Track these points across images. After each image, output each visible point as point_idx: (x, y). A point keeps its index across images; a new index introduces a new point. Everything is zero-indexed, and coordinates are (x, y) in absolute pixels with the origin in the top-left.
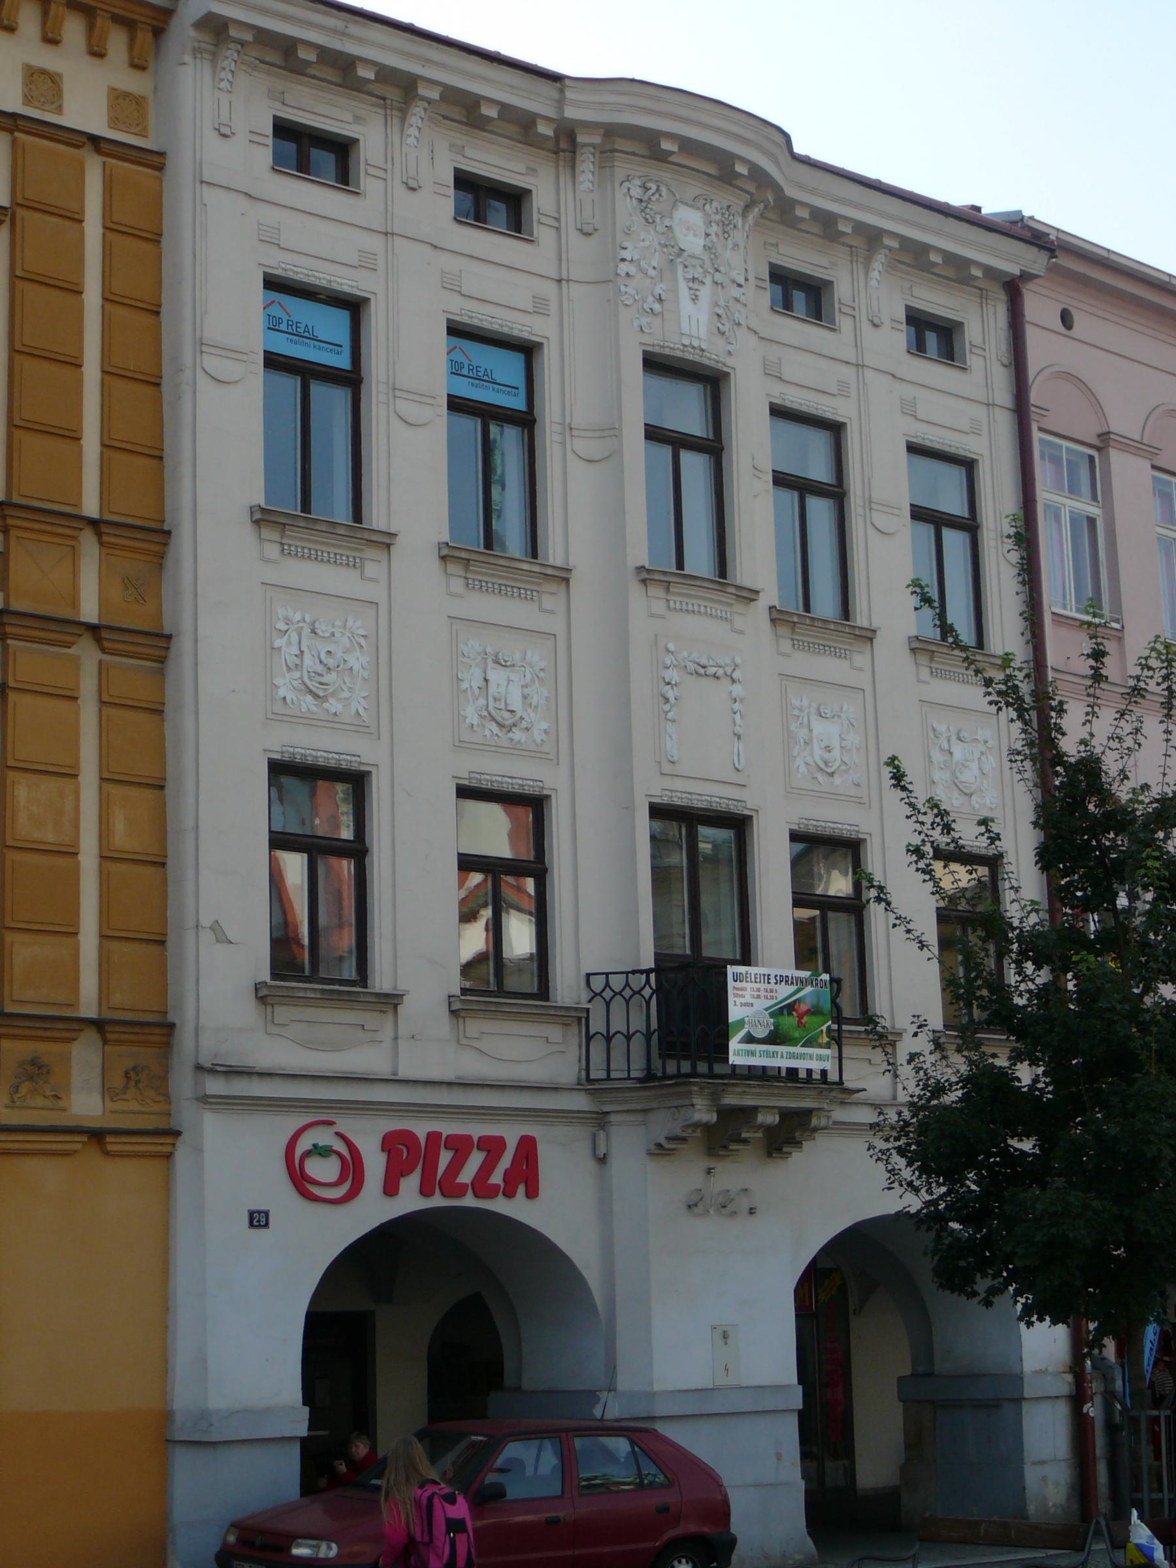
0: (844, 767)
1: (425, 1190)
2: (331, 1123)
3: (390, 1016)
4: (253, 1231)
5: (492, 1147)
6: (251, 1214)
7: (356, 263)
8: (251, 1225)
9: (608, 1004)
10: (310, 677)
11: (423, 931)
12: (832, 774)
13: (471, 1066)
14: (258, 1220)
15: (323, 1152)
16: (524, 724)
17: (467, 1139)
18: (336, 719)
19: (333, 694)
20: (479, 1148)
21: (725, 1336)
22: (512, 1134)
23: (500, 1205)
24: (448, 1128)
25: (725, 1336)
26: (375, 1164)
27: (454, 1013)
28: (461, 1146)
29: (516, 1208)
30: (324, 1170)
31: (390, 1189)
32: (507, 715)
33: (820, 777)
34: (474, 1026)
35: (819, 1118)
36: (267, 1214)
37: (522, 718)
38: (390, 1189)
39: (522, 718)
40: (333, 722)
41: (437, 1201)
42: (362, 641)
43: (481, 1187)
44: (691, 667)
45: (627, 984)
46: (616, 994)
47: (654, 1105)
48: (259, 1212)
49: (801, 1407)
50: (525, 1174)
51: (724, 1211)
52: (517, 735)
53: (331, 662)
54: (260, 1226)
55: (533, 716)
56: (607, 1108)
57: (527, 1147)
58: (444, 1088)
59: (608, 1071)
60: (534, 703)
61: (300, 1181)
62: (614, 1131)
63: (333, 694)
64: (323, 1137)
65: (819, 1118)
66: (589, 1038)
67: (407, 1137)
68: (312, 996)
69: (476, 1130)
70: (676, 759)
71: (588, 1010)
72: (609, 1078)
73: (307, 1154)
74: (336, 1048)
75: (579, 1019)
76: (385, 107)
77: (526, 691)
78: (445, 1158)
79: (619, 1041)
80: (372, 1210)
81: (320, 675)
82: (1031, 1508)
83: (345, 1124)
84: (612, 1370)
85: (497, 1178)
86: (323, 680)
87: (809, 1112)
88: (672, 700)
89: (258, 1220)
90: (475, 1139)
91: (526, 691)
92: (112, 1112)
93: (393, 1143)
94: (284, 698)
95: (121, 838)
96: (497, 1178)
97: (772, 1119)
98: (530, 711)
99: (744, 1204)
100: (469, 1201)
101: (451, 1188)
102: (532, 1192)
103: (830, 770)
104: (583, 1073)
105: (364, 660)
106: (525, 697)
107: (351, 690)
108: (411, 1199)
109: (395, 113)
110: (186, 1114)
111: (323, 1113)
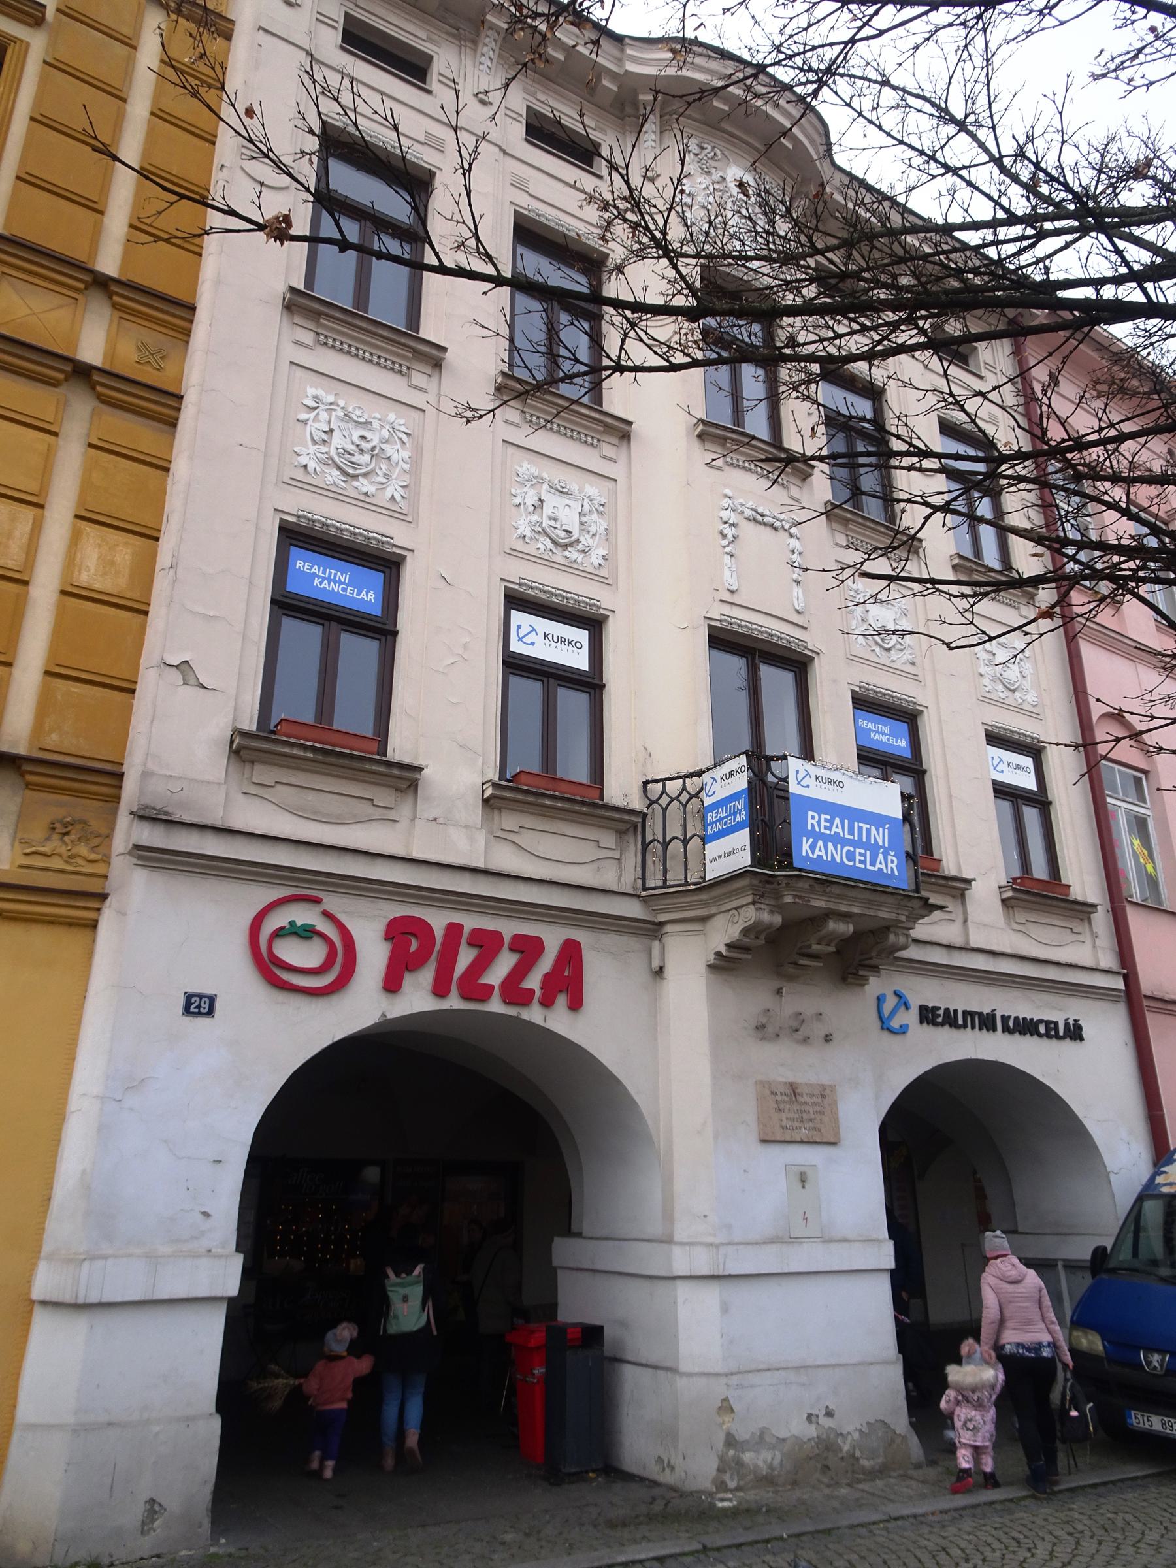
0: (898, 646)
1: (440, 989)
2: (317, 901)
3: (410, 799)
4: (188, 1019)
5: (529, 949)
6: (189, 998)
7: (422, 140)
8: (187, 1011)
9: (665, 810)
10: (338, 454)
11: (446, 707)
12: (888, 650)
13: (506, 859)
14: (199, 1006)
15: (307, 933)
16: (580, 547)
17: (497, 936)
18: (367, 500)
19: (365, 475)
20: (511, 949)
21: (803, 1179)
22: (553, 938)
23: (534, 1014)
24: (470, 922)
25: (803, 1179)
26: (373, 954)
27: (486, 802)
28: (488, 944)
29: (558, 1020)
30: (302, 954)
31: (392, 984)
32: (563, 534)
33: (878, 650)
34: (510, 821)
35: (897, 935)
36: (212, 999)
37: (578, 541)
38: (392, 984)
39: (578, 541)
40: (365, 502)
41: (454, 1002)
42: (404, 437)
43: (514, 992)
44: (748, 513)
45: (684, 788)
46: (672, 800)
47: (713, 910)
48: (201, 996)
49: (892, 1266)
50: (567, 982)
51: (796, 1035)
52: (573, 554)
53: (366, 446)
54: (200, 1014)
55: (590, 541)
56: (662, 918)
57: (571, 953)
58: (467, 875)
59: (665, 881)
60: (593, 529)
61: (270, 969)
62: (669, 941)
63: (365, 475)
64: (303, 916)
65: (897, 935)
66: (645, 846)
67: (421, 928)
68: (302, 753)
69: (509, 928)
70: (734, 588)
71: (645, 815)
72: (665, 886)
73: (278, 933)
74: (338, 822)
75: (635, 827)
76: (459, 39)
77: (584, 519)
78: (465, 957)
79: (676, 847)
80: (362, 1007)
81: (350, 454)
82: (18, 800)
83: (333, 903)
84: (669, 1216)
85: (533, 982)
86: (353, 459)
87: (886, 928)
88: (730, 536)
89: (199, 1006)
90: (507, 938)
91: (584, 519)
92: (21, 866)
93: (397, 931)
94: (305, 466)
95: (89, 575)
96: (533, 982)
97: (845, 928)
98: (588, 537)
99: (819, 1030)
100: (495, 1005)
101: (474, 990)
102: (576, 1004)
103: (886, 646)
104: (640, 882)
105: (405, 454)
106: (582, 524)
107: (386, 476)
108: (417, 998)
109: (469, 44)
110: (121, 867)
111: (307, 886)
